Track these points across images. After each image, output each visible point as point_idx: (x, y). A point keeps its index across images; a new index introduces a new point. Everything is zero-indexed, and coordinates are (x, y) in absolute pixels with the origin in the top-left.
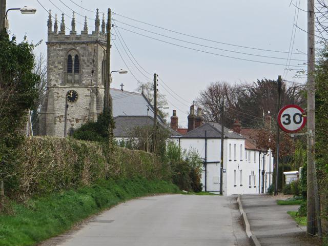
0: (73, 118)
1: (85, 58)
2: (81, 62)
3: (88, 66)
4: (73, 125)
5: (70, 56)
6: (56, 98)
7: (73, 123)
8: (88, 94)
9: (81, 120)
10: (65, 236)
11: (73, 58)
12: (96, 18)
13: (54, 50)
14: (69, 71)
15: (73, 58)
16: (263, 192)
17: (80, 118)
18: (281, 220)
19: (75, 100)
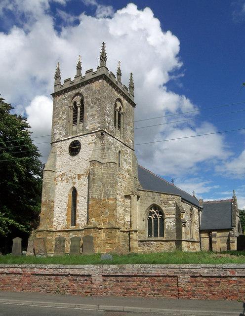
0: (75, 175)
1: (89, 100)
2: (85, 106)
3: (92, 107)
4: (74, 183)
5: (75, 103)
6: (58, 153)
7: (75, 180)
8: (91, 142)
9: (83, 175)
10: (171, 92)
11: (78, 103)
12: (101, 51)
13: (60, 100)
14: (75, 121)
15: (78, 103)
16: (74, 222)
17: (82, 173)
18: (244, 251)
19: (78, 151)
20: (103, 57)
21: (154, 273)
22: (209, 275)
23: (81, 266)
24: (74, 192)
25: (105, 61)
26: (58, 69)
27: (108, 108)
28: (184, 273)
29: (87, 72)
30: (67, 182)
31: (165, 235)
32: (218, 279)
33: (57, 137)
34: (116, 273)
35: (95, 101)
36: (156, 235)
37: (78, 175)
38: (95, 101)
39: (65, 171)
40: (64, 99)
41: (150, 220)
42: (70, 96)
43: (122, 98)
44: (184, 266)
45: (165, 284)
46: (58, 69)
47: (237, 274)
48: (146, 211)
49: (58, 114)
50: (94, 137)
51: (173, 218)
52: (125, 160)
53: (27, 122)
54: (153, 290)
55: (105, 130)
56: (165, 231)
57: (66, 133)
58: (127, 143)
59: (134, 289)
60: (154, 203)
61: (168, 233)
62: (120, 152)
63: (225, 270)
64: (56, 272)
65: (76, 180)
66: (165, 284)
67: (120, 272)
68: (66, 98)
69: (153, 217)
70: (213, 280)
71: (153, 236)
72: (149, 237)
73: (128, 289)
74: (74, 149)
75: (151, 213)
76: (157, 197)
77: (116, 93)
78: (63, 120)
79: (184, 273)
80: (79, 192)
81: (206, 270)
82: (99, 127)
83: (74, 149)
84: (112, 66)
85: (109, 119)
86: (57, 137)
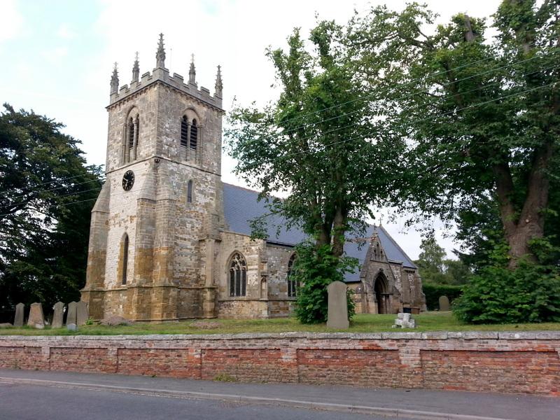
3: (147, 126)
4: (126, 228)
12: (158, 46)
20: (161, 55)
21: (89, 345)
22: (132, 347)
23: (35, 337)
24: (127, 239)
25: (163, 60)
26: (116, 72)
27: (167, 126)
28: (113, 345)
29: (144, 76)
30: (120, 226)
31: (247, 294)
32: (139, 352)
33: (111, 166)
34: (61, 345)
35: (150, 117)
36: (238, 294)
37: (131, 217)
38: (150, 117)
39: (118, 212)
40: (119, 114)
41: (232, 272)
42: (125, 109)
43: (195, 105)
44: (113, 337)
45: (98, 357)
46: (116, 72)
47: (153, 347)
48: (228, 261)
49: (113, 135)
50: (147, 166)
51: (256, 269)
52: (201, 192)
53: (255, 90)
54: (89, 363)
55: (162, 156)
56: (247, 288)
57: (121, 161)
58: (205, 167)
59: (74, 363)
60: (236, 249)
61: (250, 290)
62: (191, 182)
63: (145, 341)
64: (14, 345)
65: (128, 224)
66: (98, 357)
67: (64, 344)
68: (121, 113)
69: (235, 269)
70: (136, 353)
71: (235, 294)
72: (231, 296)
73: (70, 363)
74: (129, 180)
75: (234, 264)
76: (239, 242)
77: (184, 101)
78: (118, 143)
79: (113, 345)
80: (130, 239)
81: (130, 342)
82: (153, 152)
83: (129, 180)
84: (177, 66)
85: (169, 139)
86: (111, 166)
